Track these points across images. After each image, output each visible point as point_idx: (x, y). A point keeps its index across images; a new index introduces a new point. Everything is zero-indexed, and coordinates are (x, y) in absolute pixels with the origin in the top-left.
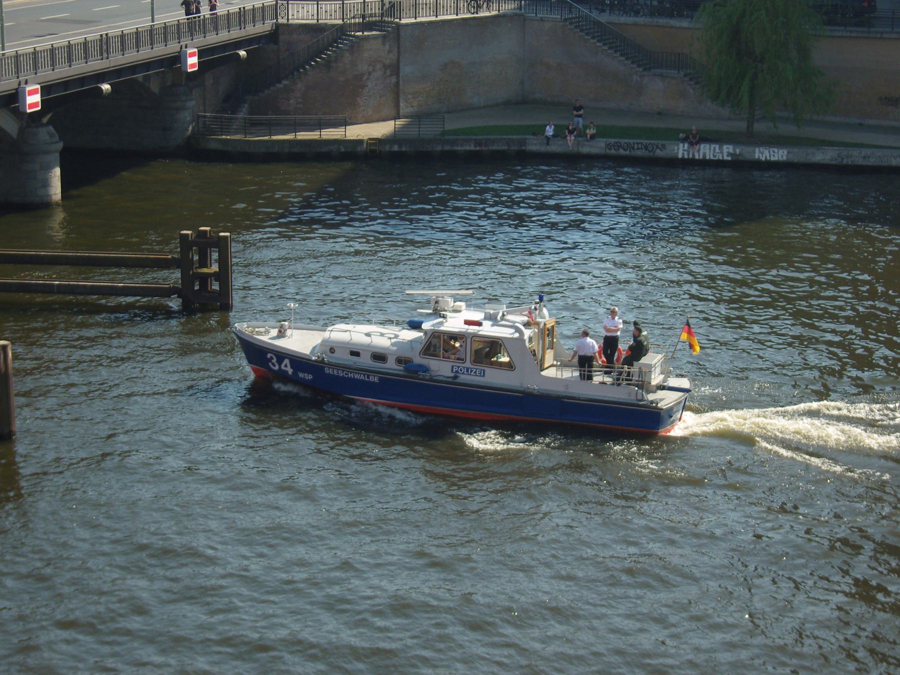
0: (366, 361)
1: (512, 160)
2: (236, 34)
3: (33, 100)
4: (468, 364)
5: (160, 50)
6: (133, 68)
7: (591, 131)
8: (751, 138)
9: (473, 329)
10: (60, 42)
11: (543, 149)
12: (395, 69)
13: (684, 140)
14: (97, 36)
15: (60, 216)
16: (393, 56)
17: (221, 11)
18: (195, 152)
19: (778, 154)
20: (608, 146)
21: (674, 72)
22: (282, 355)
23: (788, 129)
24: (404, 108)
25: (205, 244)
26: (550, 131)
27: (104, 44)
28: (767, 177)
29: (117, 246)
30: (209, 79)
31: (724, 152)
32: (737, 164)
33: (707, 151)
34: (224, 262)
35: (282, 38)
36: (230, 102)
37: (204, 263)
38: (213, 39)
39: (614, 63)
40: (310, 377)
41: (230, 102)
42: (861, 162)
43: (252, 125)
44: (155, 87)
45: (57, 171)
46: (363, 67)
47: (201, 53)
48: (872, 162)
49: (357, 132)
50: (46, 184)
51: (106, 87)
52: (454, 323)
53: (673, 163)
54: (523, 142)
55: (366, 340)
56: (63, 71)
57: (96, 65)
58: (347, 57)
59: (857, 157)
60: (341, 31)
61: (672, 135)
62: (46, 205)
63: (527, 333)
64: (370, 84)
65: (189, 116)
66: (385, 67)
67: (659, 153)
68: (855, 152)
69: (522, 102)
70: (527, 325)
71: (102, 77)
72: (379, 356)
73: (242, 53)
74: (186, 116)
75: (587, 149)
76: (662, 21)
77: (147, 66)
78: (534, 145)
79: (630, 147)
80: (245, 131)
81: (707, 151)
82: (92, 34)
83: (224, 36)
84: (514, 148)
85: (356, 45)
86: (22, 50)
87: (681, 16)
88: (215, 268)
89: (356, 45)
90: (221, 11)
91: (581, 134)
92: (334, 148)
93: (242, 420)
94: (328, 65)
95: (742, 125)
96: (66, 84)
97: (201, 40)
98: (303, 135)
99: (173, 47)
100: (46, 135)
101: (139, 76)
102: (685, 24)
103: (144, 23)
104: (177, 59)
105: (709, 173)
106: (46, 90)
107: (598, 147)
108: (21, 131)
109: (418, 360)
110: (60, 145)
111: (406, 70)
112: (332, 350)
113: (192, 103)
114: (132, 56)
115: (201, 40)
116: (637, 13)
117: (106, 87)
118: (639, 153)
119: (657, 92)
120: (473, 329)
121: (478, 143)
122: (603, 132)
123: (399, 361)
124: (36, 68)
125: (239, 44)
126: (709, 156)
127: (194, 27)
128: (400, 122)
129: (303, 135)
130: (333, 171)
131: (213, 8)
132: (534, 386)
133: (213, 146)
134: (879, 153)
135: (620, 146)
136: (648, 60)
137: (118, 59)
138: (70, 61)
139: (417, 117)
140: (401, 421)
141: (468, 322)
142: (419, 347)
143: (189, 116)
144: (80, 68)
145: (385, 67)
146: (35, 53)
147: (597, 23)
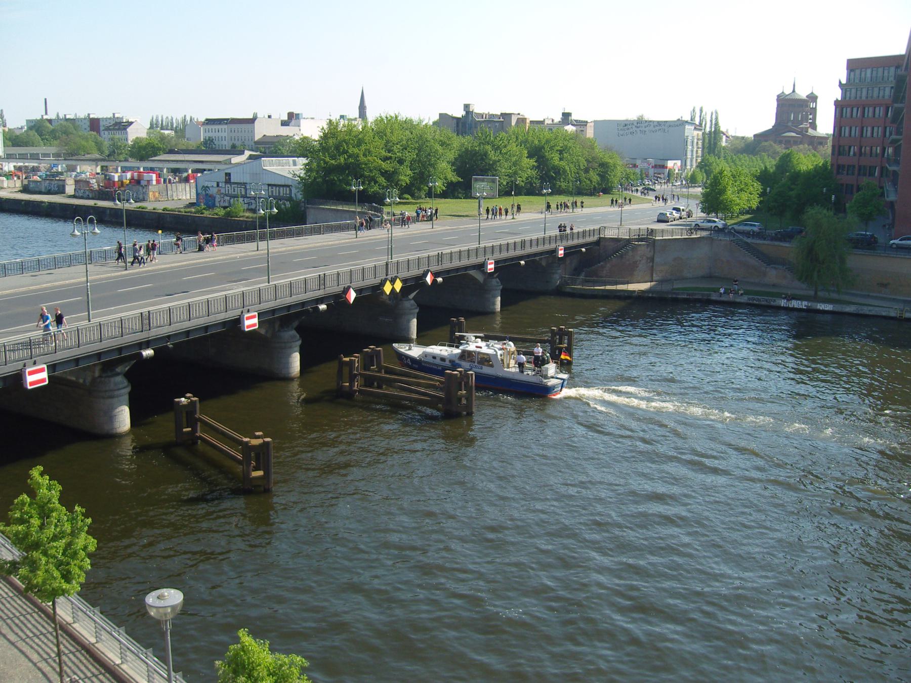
0: (438, 361)
1: (702, 303)
2: (581, 241)
3: (491, 267)
5: (547, 247)
6: (535, 255)
7: (740, 292)
8: (816, 299)
9: (478, 350)
10: (504, 242)
11: (719, 299)
12: (652, 259)
13: (784, 298)
14: (520, 240)
15: (498, 318)
16: (652, 254)
17: (575, 231)
18: (559, 292)
19: (829, 307)
20: (749, 299)
21: (781, 267)
23: (834, 296)
24: (655, 277)
25: (562, 333)
26: (722, 291)
27: (523, 243)
29: (527, 334)
30: (568, 261)
31: (803, 305)
32: (808, 310)
33: (795, 304)
34: (570, 344)
36: (577, 271)
38: (570, 243)
39: (753, 261)
41: (577, 271)
42: (867, 313)
43: (586, 282)
44: (544, 263)
45: (499, 298)
47: (565, 249)
49: (632, 287)
50: (494, 304)
51: (523, 262)
52: (472, 347)
53: (779, 308)
54: (710, 295)
55: (439, 352)
56: (504, 255)
57: (519, 252)
58: (630, 253)
59: (866, 310)
60: (628, 241)
61: (779, 296)
62: (494, 313)
63: (499, 352)
64: (640, 266)
65: (558, 277)
66: (648, 258)
67: (772, 303)
68: (865, 308)
69: (710, 277)
70: (501, 349)
71: (521, 258)
72: (443, 359)
73: (583, 250)
74: (557, 276)
75: (738, 300)
76: (777, 243)
77: (541, 253)
78: (714, 297)
79: (759, 300)
80: (582, 283)
81: (795, 304)
82: (518, 239)
83: (576, 242)
85: (635, 248)
86: (487, 245)
87: (785, 241)
88: (566, 345)
89: (635, 248)
90: (575, 231)
91: (736, 293)
92: (622, 293)
94: (621, 256)
95: (812, 293)
96: (505, 260)
97: (565, 243)
98: (608, 287)
99: (553, 246)
100: (495, 282)
101: (537, 258)
102: (787, 245)
103: (541, 235)
104: (555, 251)
106: (496, 262)
107: (744, 299)
108: (485, 280)
109: (457, 361)
111: (657, 260)
114: (535, 249)
115: (565, 243)
116: (765, 239)
117: (523, 262)
118: (763, 303)
119: (773, 275)
120: (478, 350)
121: (688, 295)
122: (747, 293)
123: (450, 361)
124: (493, 253)
125: (582, 246)
127: (562, 238)
128: (653, 283)
129: (608, 287)
130: (620, 304)
131: (572, 229)
132: (500, 374)
133: (568, 290)
134: (877, 309)
135: (754, 299)
136: (770, 261)
137: (528, 250)
139: (661, 282)
143: (558, 277)
144: (512, 253)
145: (648, 258)
146: (500, 245)
147: (747, 243)
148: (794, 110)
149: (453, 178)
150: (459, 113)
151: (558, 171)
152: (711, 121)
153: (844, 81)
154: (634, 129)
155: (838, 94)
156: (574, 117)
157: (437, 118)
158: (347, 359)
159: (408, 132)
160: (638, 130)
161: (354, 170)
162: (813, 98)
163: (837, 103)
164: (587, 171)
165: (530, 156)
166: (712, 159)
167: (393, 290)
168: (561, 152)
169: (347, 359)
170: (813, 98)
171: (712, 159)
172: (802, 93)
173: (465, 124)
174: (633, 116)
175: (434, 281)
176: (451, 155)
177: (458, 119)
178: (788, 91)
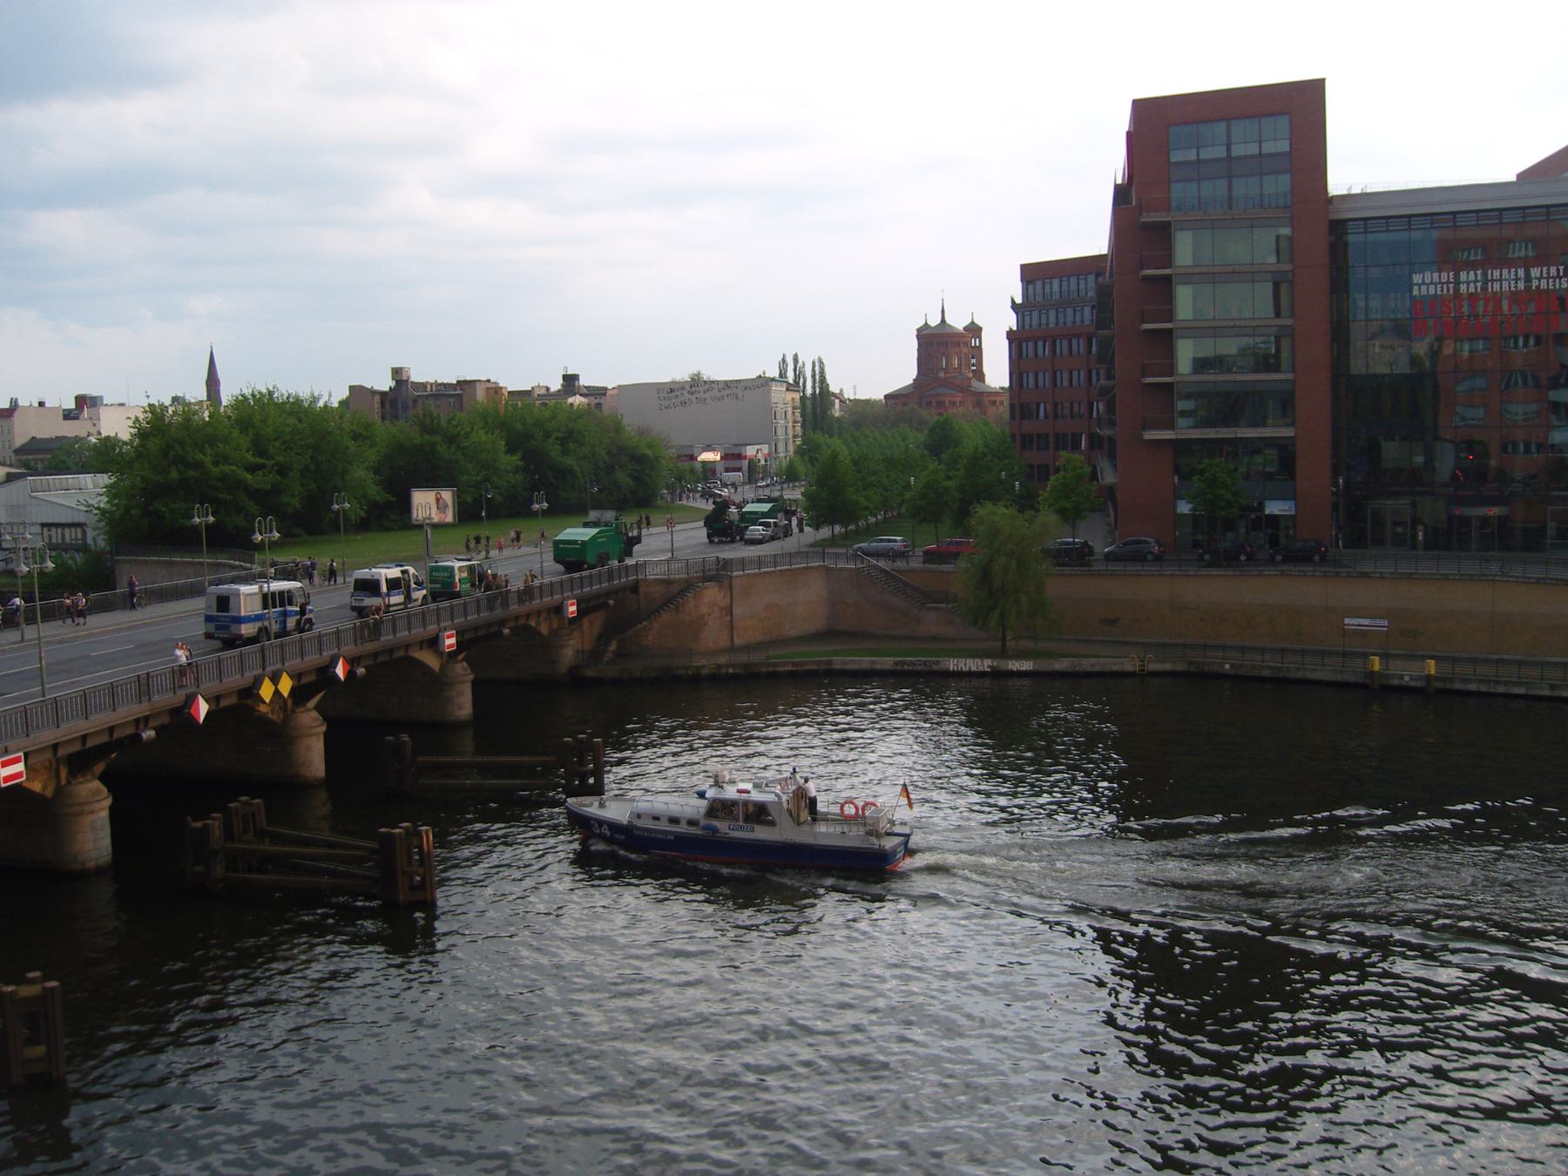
0: (664, 826)
3: (450, 642)
4: (741, 823)
8: (1004, 654)
19: (1027, 666)
22: (601, 822)
28: (1019, 682)
31: (986, 664)
32: (996, 674)
35: (642, 590)
37: (582, 762)
40: (1268, 923)
42: (1089, 669)
44: (544, 630)
46: (704, 610)
48: (1097, 668)
53: (948, 674)
59: (1086, 664)
66: (721, 609)
79: (913, 663)
84: (823, 667)
93: (1154, 964)
105: (975, 682)
106: (460, 634)
108: (442, 667)
110: (471, 677)
111: (737, 611)
112: (639, 816)
113: (572, 642)
121: (795, 664)
126: (974, 668)
138: (478, 612)
140: (1323, 956)
141: (739, 791)
142: (703, 811)
145: (721, 609)
148: (944, 349)
149: (375, 492)
150: (385, 383)
151: (564, 474)
152: (813, 376)
153: (1019, 300)
154: (687, 396)
155: (1011, 321)
156: (584, 381)
157: (345, 394)
158: (198, 824)
159: (292, 421)
160: (693, 397)
161: (198, 490)
162: (974, 330)
163: (1011, 335)
164: (610, 470)
165: (511, 450)
166: (819, 437)
167: (277, 693)
168: (563, 442)
169: (198, 824)
170: (974, 330)
171: (819, 437)
172: (958, 322)
173: (402, 396)
174: (682, 375)
175: (350, 674)
176: (372, 456)
177: (383, 394)
178: (934, 321)
